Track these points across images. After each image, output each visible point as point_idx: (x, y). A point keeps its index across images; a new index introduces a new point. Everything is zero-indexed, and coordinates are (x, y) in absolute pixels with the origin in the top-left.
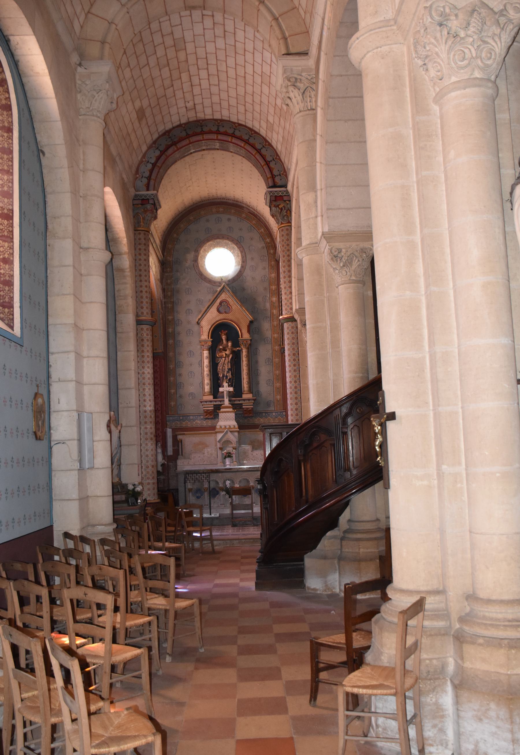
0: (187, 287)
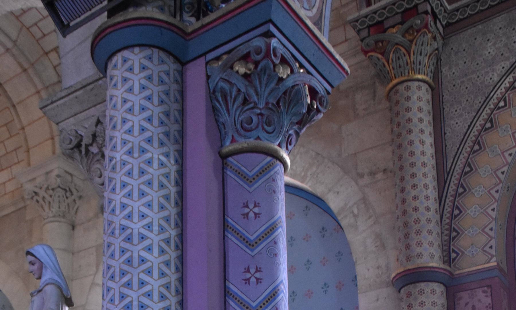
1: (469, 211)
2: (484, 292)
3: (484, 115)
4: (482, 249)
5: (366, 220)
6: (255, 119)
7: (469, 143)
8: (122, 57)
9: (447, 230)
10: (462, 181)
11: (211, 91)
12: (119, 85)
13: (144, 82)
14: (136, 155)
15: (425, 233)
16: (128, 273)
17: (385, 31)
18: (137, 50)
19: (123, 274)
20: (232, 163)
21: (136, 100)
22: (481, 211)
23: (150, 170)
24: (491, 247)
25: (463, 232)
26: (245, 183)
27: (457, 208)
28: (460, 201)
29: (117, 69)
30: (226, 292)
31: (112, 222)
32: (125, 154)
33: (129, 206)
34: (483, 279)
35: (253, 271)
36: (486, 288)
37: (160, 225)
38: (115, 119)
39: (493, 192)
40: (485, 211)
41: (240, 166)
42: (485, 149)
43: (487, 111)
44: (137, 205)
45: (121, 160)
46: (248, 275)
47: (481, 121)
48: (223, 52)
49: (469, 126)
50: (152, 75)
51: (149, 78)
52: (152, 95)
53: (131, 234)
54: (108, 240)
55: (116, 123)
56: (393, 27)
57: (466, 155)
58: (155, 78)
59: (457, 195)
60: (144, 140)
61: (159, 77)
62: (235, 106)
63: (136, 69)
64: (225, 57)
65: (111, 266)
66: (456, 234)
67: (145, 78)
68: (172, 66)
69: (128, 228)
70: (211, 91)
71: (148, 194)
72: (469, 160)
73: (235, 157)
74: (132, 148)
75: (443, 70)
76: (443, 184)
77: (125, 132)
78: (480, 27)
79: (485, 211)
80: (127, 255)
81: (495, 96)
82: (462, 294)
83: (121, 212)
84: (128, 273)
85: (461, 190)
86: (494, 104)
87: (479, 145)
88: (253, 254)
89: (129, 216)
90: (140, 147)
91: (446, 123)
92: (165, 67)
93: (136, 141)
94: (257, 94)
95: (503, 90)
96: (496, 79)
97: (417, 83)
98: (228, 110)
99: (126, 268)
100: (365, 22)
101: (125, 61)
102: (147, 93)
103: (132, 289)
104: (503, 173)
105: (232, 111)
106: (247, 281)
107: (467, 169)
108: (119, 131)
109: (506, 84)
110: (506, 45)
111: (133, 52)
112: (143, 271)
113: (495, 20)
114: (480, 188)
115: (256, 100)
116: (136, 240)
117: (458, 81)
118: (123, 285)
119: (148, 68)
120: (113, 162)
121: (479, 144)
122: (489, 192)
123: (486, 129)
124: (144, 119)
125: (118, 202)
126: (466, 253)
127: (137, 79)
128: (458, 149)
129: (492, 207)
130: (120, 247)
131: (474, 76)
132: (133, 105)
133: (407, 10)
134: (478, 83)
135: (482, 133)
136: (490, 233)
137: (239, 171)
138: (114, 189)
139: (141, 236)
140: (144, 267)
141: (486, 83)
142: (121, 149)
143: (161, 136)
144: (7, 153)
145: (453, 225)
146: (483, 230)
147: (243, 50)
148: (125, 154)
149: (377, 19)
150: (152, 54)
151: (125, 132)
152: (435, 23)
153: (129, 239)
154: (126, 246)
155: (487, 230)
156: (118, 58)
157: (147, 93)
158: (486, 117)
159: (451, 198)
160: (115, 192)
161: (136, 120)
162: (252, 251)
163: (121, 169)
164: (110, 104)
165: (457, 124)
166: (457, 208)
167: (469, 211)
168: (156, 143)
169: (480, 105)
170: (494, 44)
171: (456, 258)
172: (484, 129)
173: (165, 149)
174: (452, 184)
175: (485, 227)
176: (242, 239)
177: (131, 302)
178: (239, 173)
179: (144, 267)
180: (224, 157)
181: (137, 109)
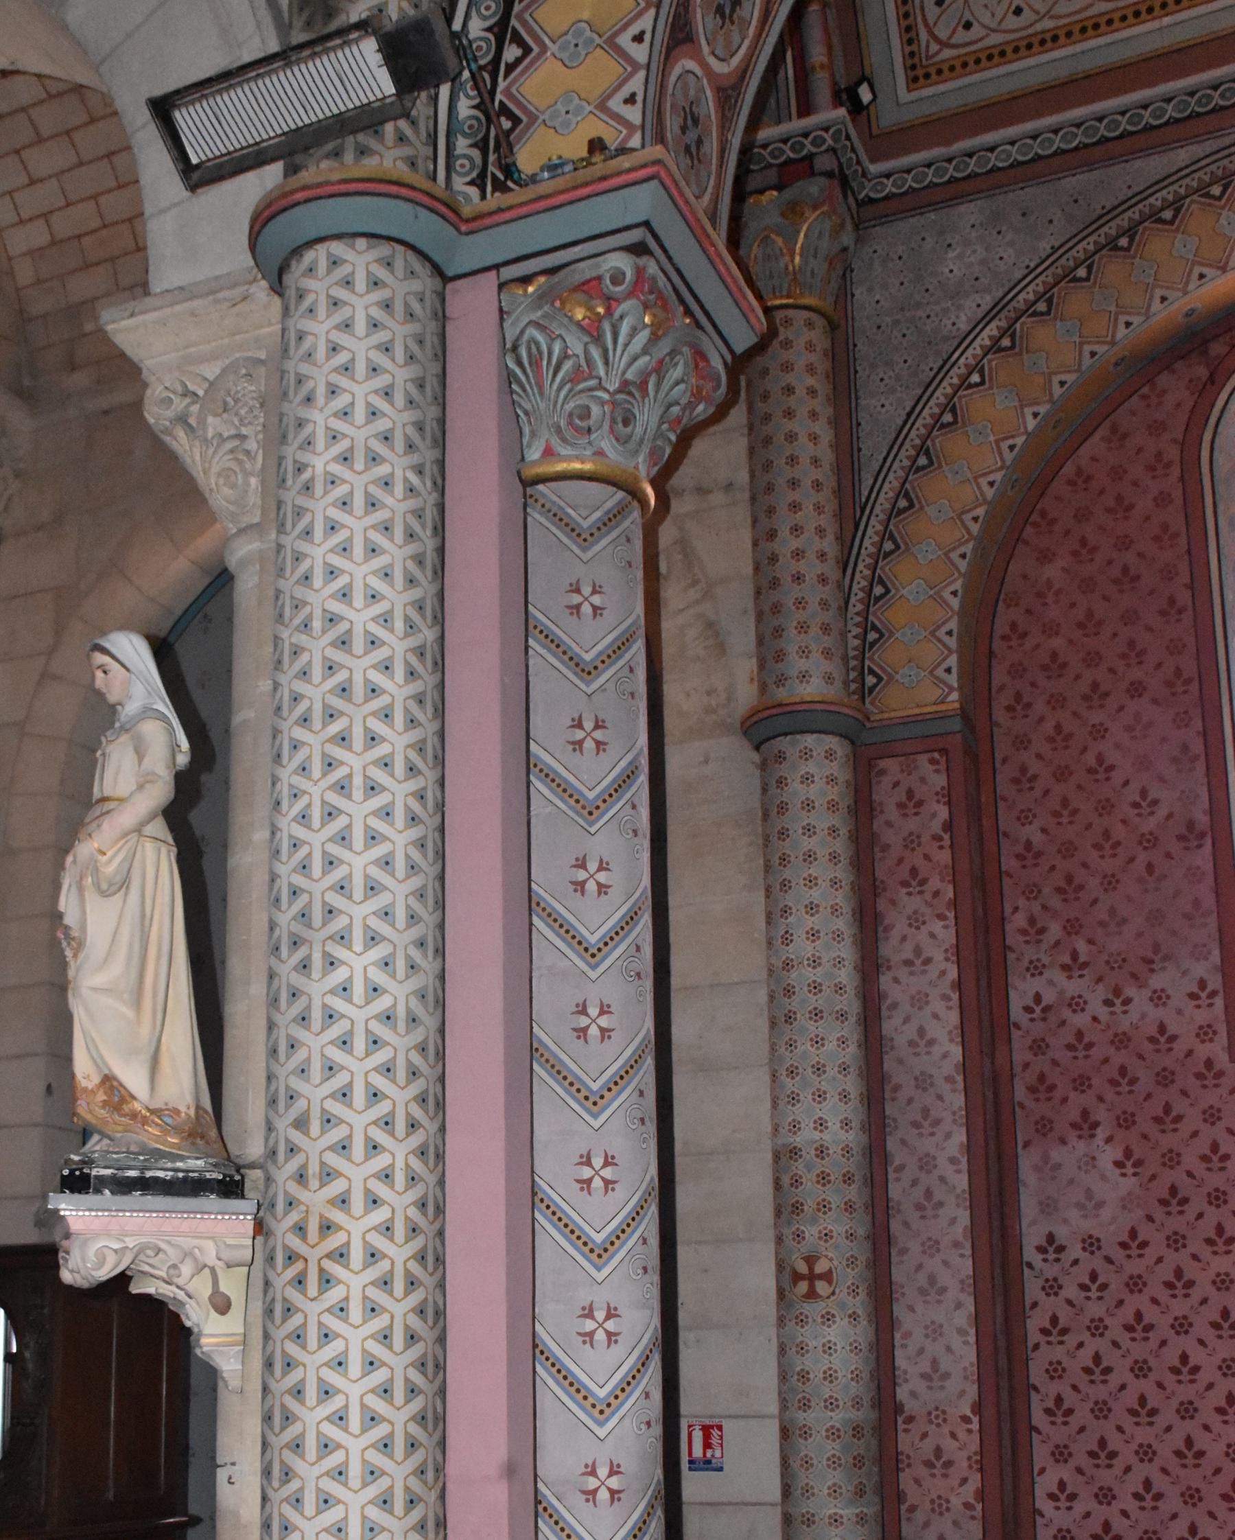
1: (904, 592)
2: (933, 761)
3: (940, 397)
4: (931, 672)
5: (686, 589)
6: (595, 410)
7: (908, 450)
8: (329, 255)
9: (857, 625)
10: (891, 527)
11: (508, 346)
12: (322, 311)
13: (377, 313)
14: (359, 466)
16: (342, 714)
18: (361, 243)
19: (331, 715)
20: (544, 496)
21: (360, 347)
23: (389, 501)
24: (948, 671)
26: (575, 543)
27: (881, 582)
29: (316, 278)
30: (529, 763)
31: (305, 603)
32: (335, 459)
33: (343, 572)
34: (922, 736)
35: (588, 725)
36: (936, 755)
37: (407, 618)
38: (311, 384)
39: (954, 556)
40: (938, 593)
41: (562, 504)
42: (940, 466)
43: (946, 388)
44: (360, 573)
45: (327, 473)
46: (579, 734)
47: (932, 408)
48: (537, 269)
49: (909, 415)
50: (392, 299)
51: (387, 306)
52: (392, 341)
53: (349, 632)
54: (294, 640)
55: (313, 391)
57: (901, 473)
58: (399, 307)
59: (880, 555)
60: (376, 436)
61: (406, 304)
62: (558, 379)
63: (361, 284)
64: (542, 279)
65: (302, 696)
67: (377, 304)
68: (425, 282)
69: (342, 618)
70: (508, 346)
71: (384, 552)
72: (907, 485)
73: (553, 485)
74: (352, 449)
75: (857, 292)
76: (852, 527)
77: (335, 415)
78: (932, 216)
79: (938, 593)
80: (341, 676)
81: (962, 360)
82: (883, 764)
83: (325, 584)
84: (342, 714)
85: (888, 546)
86: (959, 376)
87: (927, 458)
88: (589, 690)
89: (345, 595)
90: (368, 449)
91: (862, 402)
92: (416, 285)
93: (360, 436)
94: (606, 363)
95: (979, 351)
96: (964, 326)
97: (806, 314)
98: (541, 388)
99: (337, 703)
101: (335, 263)
102: (382, 336)
103: (350, 749)
104: (975, 519)
105: (550, 391)
106: (578, 745)
107: (903, 503)
108: (321, 410)
109: (984, 339)
110: (983, 262)
111: (353, 247)
112: (374, 714)
113: (962, 208)
114: (929, 544)
115: (602, 373)
116: (358, 644)
117: (888, 320)
118: (331, 740)
119: (385, 285)
120: (306, 475)
121: (927, 453)
123: (943, 426)
124: (376, 392)
125: (319, 562)
126: (897, 677)
127: (362, 306)
128: (885, 459)
129: (952, 588)
130: (324, 658)
131: (921, 313)
132: (353, 359)
133: (789, 162)
134: (928, 328)
135: (935, 433)
136: (946, 639)
137: (560, 515)
138: (308, 533)
139: (371, 638)
140: (376, 704)
141: (945, 333)
142: (326, 449)
143: (410, 430)
145: (871, 618)
146: (933, 633)
147: (585, 270)
148: (335, 459)
150: (393, 256)
151: (335, 415)
152: (845, 197)
153: (343, 643)
154: (338, 656)
155: (941, 633)
156: (319, 255)
157: (382, 336)
158: (942, 400)
159: (869, 561)
161: (360, 392)
162: (588, 684)
163: (326, 493)
164: (297, 348)
165: (882, 407)
166: (881, 582)
167: (904, 592)
168: (399, 445)
169: (932, 374)
170: (960, 257)
171: (875, 685)
172: (938, 423)
173: (415, 459)
174: (870, 531)
175: (939, 627)
176: (566, 658)
177: (350, 776)
178: (559, 519)
179: (376, 704)
180: (528, 483)
181: (361, 368)
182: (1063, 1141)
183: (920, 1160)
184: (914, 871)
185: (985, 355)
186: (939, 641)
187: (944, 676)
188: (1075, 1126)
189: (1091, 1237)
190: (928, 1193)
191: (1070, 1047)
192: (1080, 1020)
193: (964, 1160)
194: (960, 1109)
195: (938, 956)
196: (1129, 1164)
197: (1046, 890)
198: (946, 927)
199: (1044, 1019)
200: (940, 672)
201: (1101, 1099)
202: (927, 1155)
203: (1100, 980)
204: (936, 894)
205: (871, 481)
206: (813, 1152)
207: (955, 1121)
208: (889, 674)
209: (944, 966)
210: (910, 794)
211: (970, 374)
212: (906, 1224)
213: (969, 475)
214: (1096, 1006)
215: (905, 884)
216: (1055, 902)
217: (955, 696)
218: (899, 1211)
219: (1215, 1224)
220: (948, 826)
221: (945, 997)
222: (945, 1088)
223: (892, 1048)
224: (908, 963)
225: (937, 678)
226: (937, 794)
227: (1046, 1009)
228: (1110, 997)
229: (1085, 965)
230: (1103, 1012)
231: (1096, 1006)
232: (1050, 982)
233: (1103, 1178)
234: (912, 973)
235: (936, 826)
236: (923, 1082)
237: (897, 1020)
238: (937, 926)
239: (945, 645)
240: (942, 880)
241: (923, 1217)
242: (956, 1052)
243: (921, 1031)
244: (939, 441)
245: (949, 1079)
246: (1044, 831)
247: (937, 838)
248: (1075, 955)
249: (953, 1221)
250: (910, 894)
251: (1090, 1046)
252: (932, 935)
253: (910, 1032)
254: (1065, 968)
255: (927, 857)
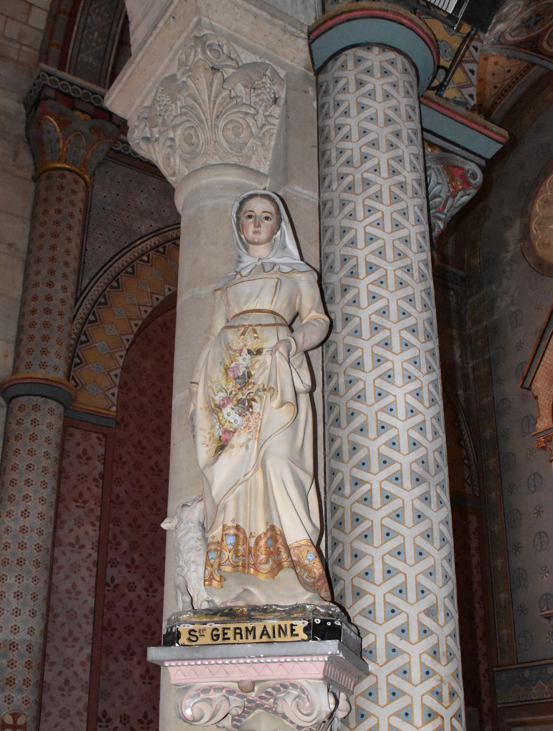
0: (513, 309)
2: (99, 439)
15: (53, 341)
17: (73, 109)
22: (109, 351)
25: (87, 364)
28: (89, 329)
36: (101, 436)
56: (84, 112)
66: (79, 361)
79: (113, 353)
81: (140, 247)
87: (115, 285)
100: (67, 88)
122: (120, 335)
144: (7, 17)
146: (108, 372)
149: (70, 90)
155: (112, 374)
160: (425, 293)
169: (125, 245)
182: (116, 659)
183: (64, 660)
184: (81, 495)
185: (151, 250)
186: (110, 377)
187: (111, 396)
188: (123, 653)
189: (125, 715)
190: (67, 681)
191: (126, 609)
192: (132, 596)
193: (89, 664)
194: (89, 634)
195: (88, 545)
196: (147, 677)
197: (124, 523)
198: (94, 530)
199: (114, 591)
200: (109, 394)
201: (137, 640)
202: (68, 658)
203: (143, 577)
204: (92, 511)
205: (88, 281)
206: (25, 648)
207: (86, 641)
208: (82, 383)
209: (91, 551)
210: (85, 452)
211: (143, 255)
212: (52, 698)
213: (136, 302)
214: (140, 590)
215: (76, 501)
216: (127, 530)
217: (114, 409)
218: (49, 690)
219: (144, 711)
220: (102, 476)
221: (89, 569)
222: (83, 621)
223: (57, 592)
224: (71, 545)
225: (106, 396)
226: (99, 456)
227: (117, 586)
228: (148, 587)
229: (137, 567)
230: (143, 594)
231: (140, 590)
232: (120, 572)
233: (135, 683)
234: (73, 551)
235: (96, 474)
236: (72, 615)
237: (61, 576)
238: (90, 529)
239: (113, 381)
240: (96, 504)
241: (63, 695)
242: (91, 601)
243: (74, 586)
244: (123, 278)
245: (85, 616)
246: (126, 492)
247: (95, 480)
248: (133, 561)
249: (79, 699)
250: (77, 506)
251: (135, 610)
252: (86, 533)
253: (67, 585)
254: (127, 566)
255: (89, 489)
